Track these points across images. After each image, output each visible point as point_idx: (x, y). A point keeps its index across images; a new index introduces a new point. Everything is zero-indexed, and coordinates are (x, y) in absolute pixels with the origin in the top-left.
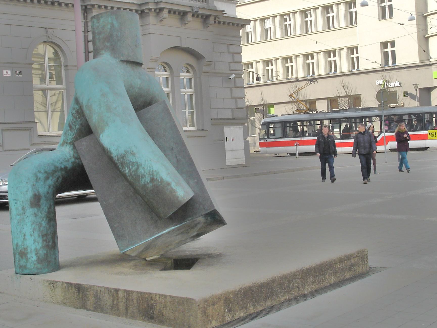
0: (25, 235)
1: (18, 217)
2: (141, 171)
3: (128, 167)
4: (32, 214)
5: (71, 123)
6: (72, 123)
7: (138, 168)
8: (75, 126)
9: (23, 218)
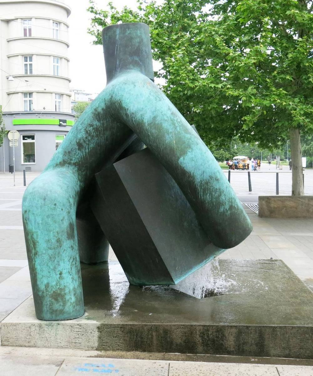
0: (61, 274)
1: (50, 252)
2: (223, 197)
3: (210, 194)
4: (69, 247)
5: (82, 141)
6: (84, 141)
7: (220, 195)
8: (89, 144)
9: (59, 253)
